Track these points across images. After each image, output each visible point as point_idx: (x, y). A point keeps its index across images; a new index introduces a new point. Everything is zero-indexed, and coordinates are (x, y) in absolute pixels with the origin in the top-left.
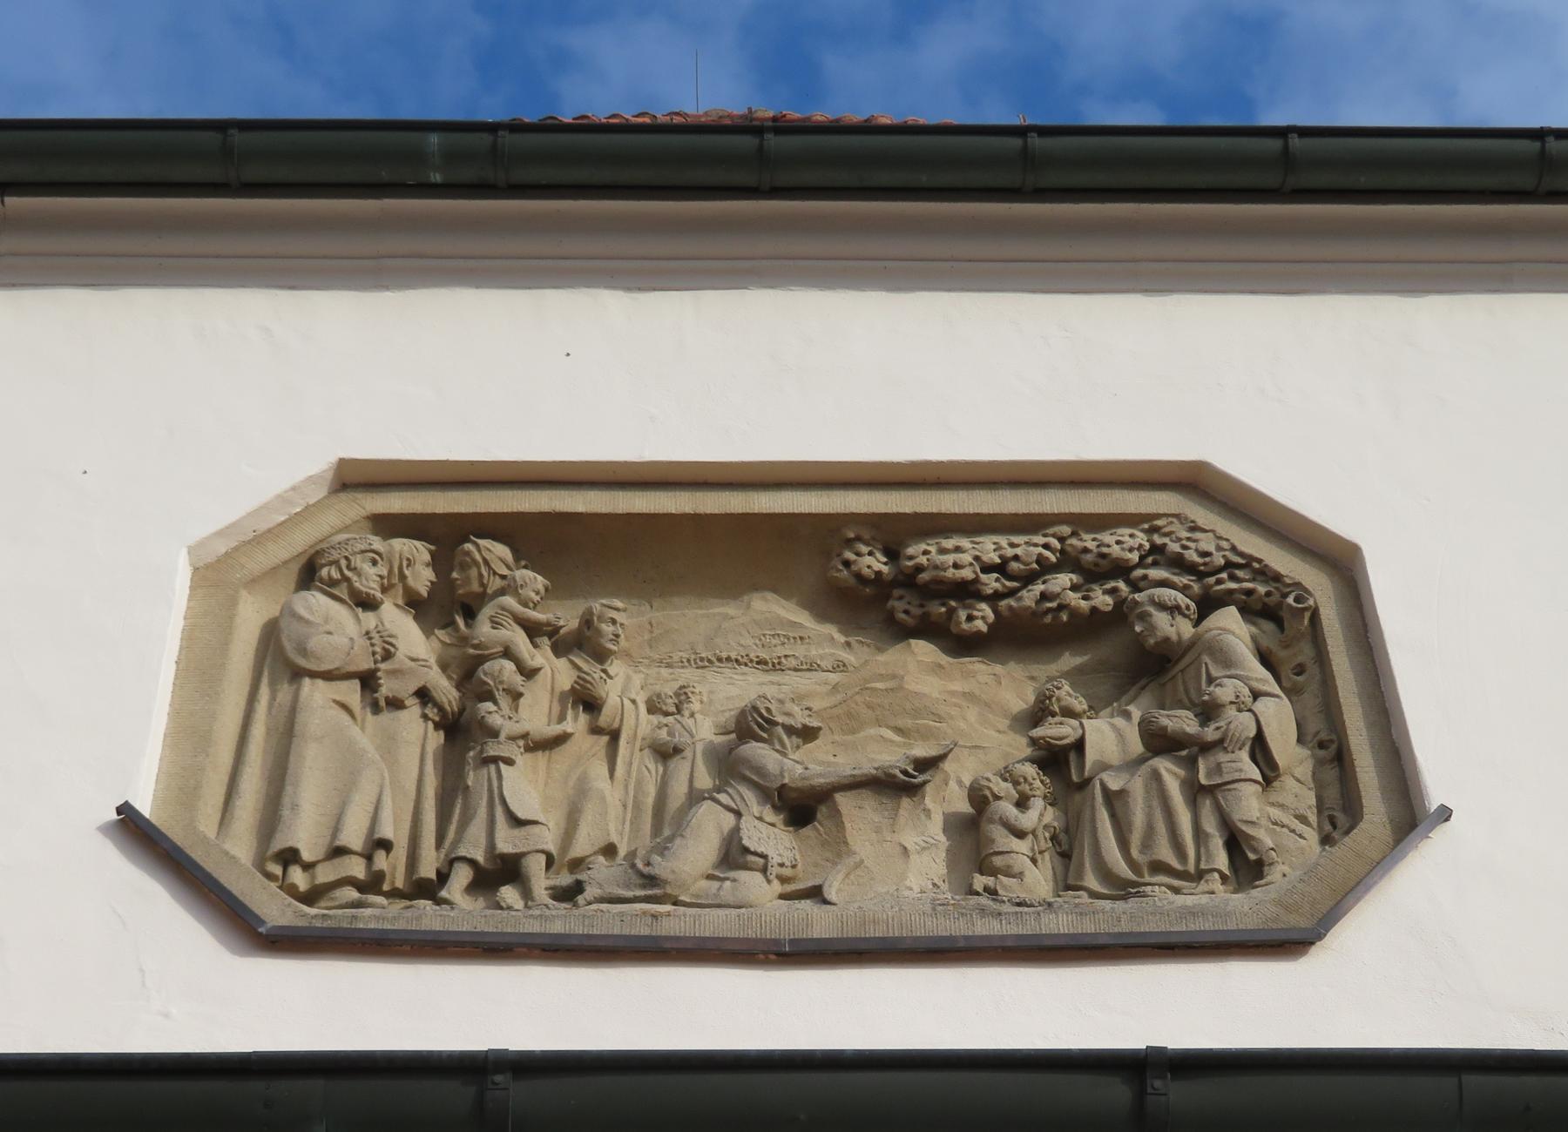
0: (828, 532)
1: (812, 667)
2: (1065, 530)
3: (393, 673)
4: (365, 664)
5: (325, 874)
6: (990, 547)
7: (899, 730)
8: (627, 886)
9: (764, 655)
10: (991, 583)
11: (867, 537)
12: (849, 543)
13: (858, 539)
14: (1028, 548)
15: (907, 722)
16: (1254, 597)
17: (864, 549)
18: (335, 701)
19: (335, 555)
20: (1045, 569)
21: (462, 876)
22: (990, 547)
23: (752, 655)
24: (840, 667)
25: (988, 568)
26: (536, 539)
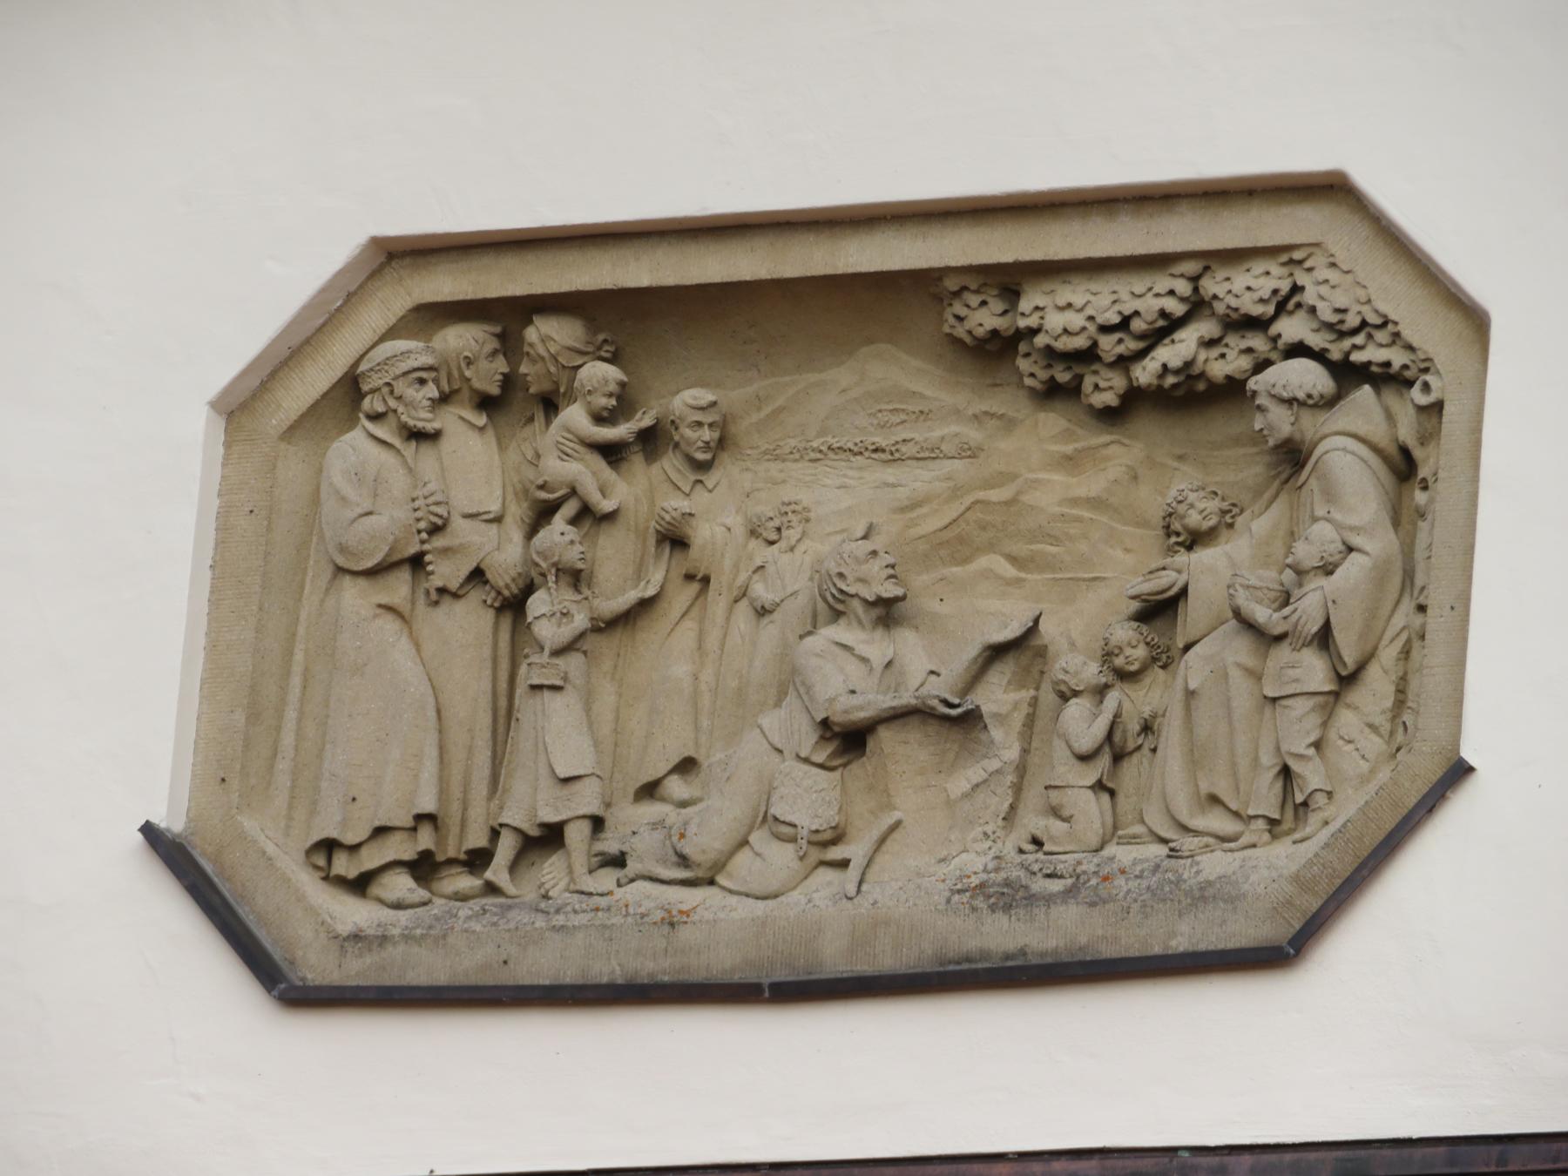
0: (925, 286)
1: (932, 454)
2: (1191, 267)
3: (446, 551)
4: (413, 549)
5: (370, 859)
6: (1102, 300)
7: (1013, 559)
8: (663, 861)
9: (881, 441)
10: (1109, 346)
11: (973, 286)
12: (957, 294)
13: (965, 288)
14: (1150, 297)
15: (1022, 549)
16: (685, 934)
17: (974, 300)
18: (380, 606)
19: (376, 381)
20: (1168, 326)
21: (506, 848)
22: (1102, 300)
23: (867, 444)
24: (970, 452)
25: (1106, 329)
26: (615, 317)
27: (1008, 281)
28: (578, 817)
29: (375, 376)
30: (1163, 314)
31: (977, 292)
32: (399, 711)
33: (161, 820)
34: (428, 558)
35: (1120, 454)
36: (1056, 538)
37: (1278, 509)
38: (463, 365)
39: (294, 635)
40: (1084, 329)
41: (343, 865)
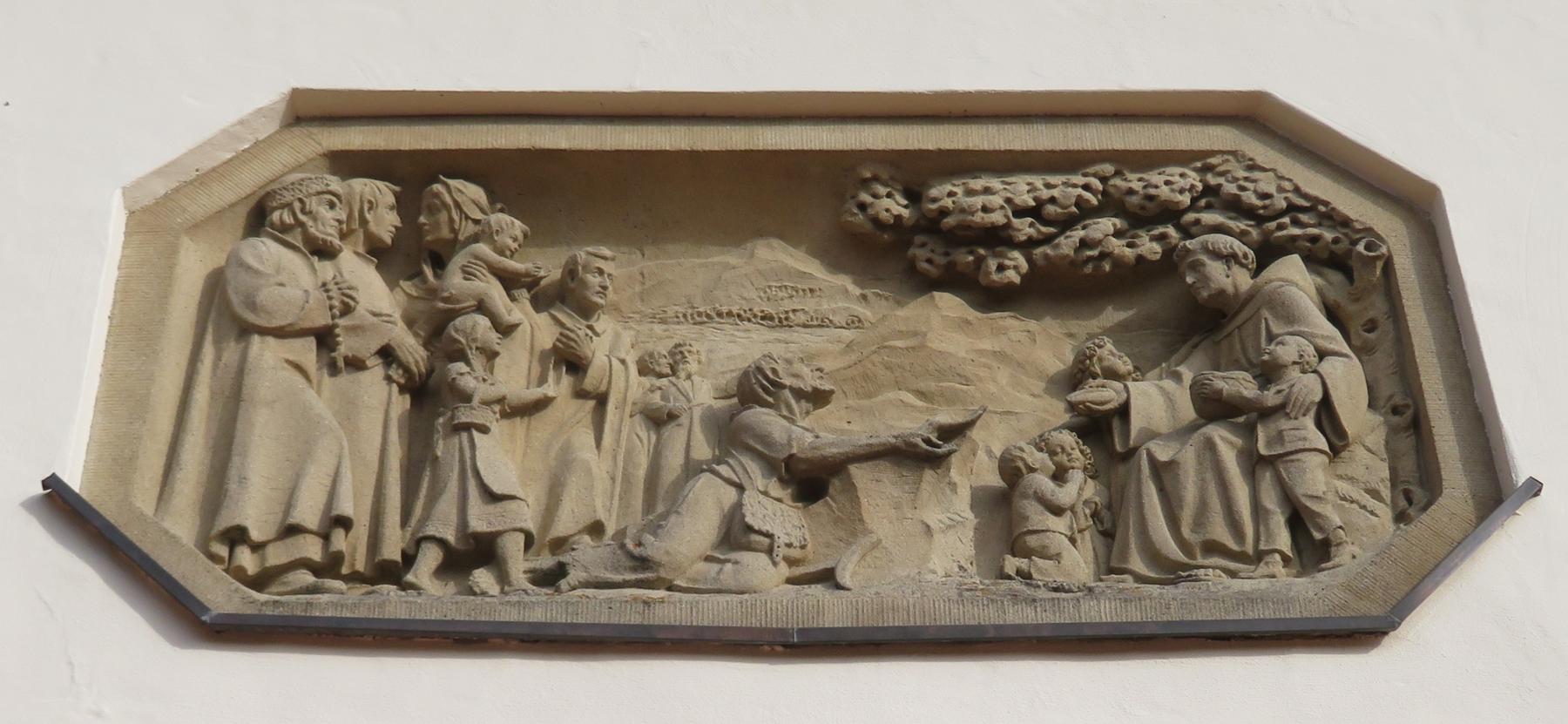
0: (843, 171)
1: (824, 323)
3: (354, 329)
4: (321, 319)
5: (277, 555)
7: (921, 394)
9: (769, 310)
10: (1025, 228)
11: (885, 176)
13: (875, 179)
14: (1066, 189)
15: (930, 385)
17: (882, 190)
18: (288, 361)
20: (1085, 212)
21: (430, 558)
23: (756, 310)
24: (855, 322)
25: (1020, 212)
26: (521, 182)
27: (913, 172)
28: (515, 530)
29: (285, 193)
30: (1080, 202)
31: (886, 185)
32: (323, 447)
33: (74, 480)
34: (337, 331)
35: (1012, 327)
36: (967, 379)
37: (998, 454)
38: (366, 207)
39: (133, 458)
40: (1002, 207)
41: (247, 560)
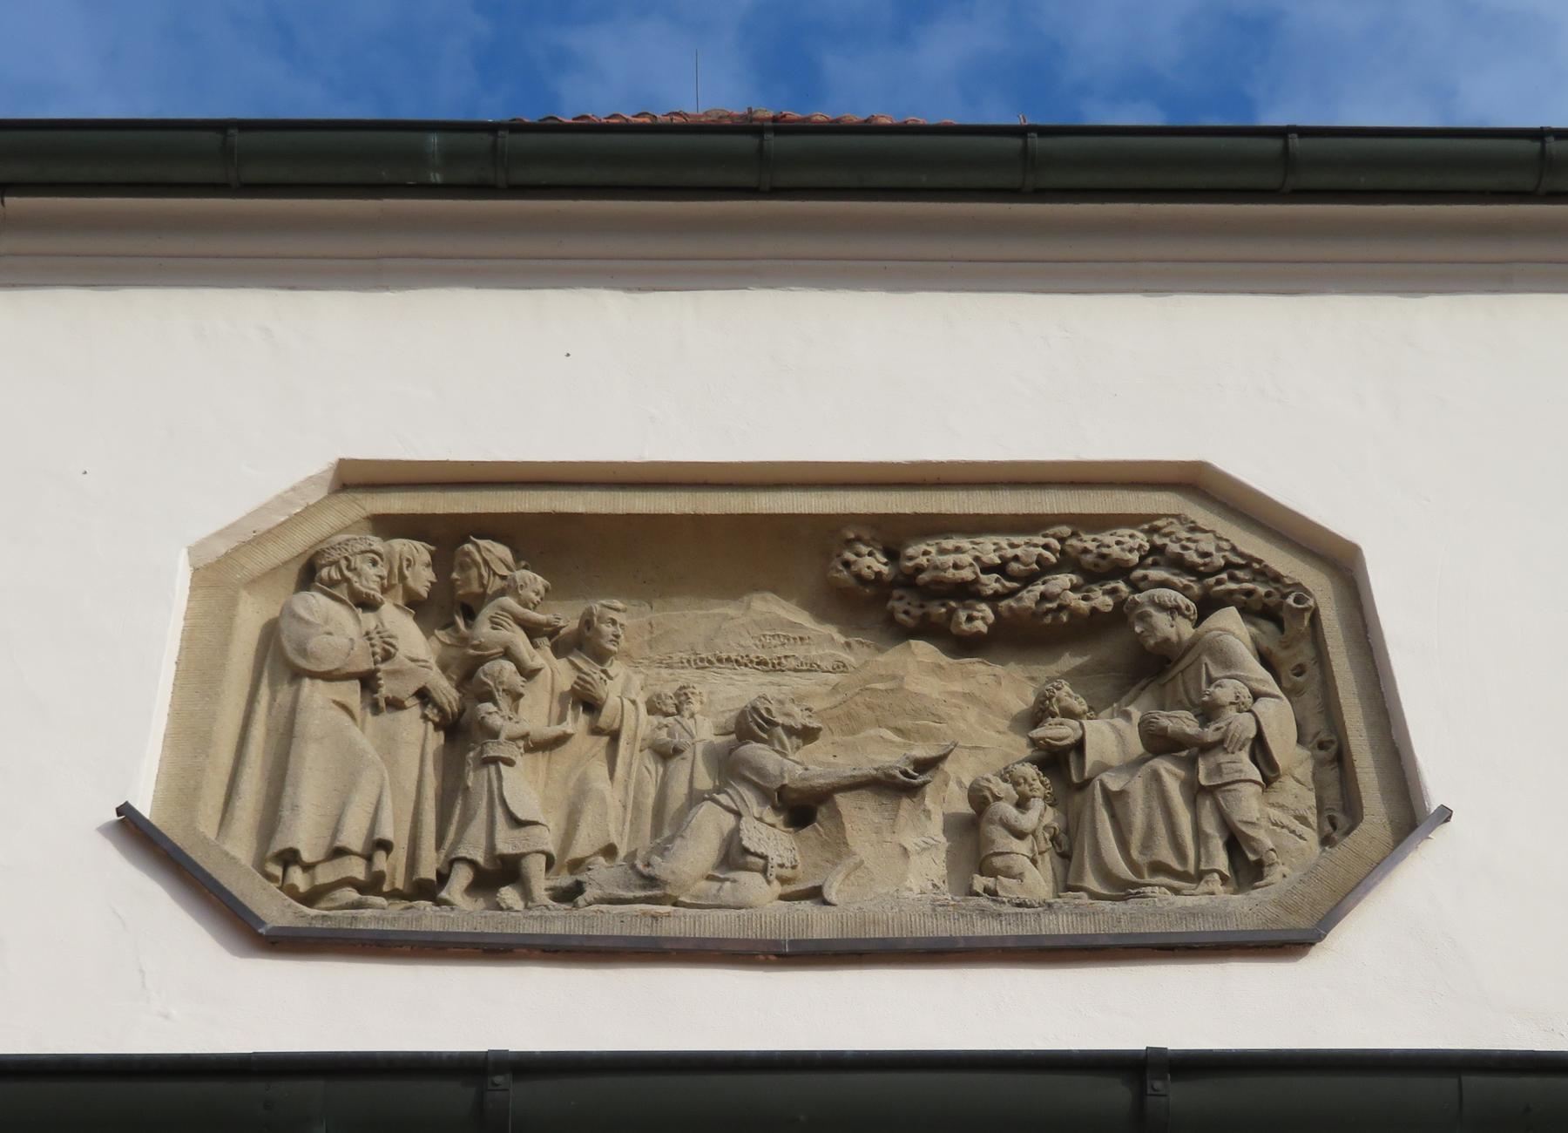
0: (828, 533)
1: (812, 668)
2: (1065, 530)
3: (393, 673)
4: (365, 665)
5: (325, 875)
6: (990, 548)
7: (899, 731)
8: (627, 887)
9: (764, 656)
10: (991, 583)
11: (867, 537)
12: (849, 543)
13: (858, 539)
14: (1028, 548)
15: (907, 723)
16: (1254, 598)
17: (864, 549)
18: (335, 702)
19: (335, 556)
20: (1045, 569)
21: (462, 877)
22: (990, 548)
23: (752, 656)
24: (840, 667)
25: (988, 569)
26: (536, 540)
